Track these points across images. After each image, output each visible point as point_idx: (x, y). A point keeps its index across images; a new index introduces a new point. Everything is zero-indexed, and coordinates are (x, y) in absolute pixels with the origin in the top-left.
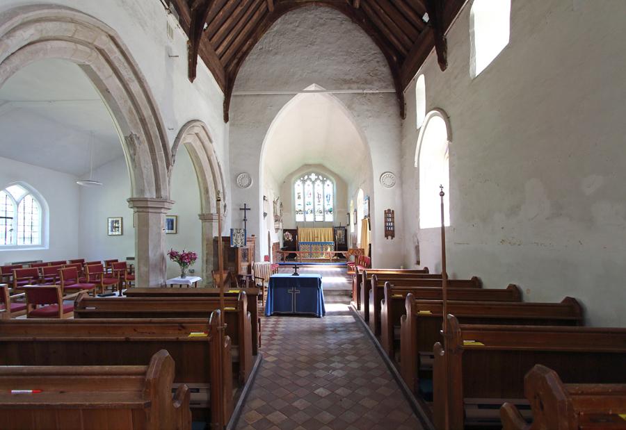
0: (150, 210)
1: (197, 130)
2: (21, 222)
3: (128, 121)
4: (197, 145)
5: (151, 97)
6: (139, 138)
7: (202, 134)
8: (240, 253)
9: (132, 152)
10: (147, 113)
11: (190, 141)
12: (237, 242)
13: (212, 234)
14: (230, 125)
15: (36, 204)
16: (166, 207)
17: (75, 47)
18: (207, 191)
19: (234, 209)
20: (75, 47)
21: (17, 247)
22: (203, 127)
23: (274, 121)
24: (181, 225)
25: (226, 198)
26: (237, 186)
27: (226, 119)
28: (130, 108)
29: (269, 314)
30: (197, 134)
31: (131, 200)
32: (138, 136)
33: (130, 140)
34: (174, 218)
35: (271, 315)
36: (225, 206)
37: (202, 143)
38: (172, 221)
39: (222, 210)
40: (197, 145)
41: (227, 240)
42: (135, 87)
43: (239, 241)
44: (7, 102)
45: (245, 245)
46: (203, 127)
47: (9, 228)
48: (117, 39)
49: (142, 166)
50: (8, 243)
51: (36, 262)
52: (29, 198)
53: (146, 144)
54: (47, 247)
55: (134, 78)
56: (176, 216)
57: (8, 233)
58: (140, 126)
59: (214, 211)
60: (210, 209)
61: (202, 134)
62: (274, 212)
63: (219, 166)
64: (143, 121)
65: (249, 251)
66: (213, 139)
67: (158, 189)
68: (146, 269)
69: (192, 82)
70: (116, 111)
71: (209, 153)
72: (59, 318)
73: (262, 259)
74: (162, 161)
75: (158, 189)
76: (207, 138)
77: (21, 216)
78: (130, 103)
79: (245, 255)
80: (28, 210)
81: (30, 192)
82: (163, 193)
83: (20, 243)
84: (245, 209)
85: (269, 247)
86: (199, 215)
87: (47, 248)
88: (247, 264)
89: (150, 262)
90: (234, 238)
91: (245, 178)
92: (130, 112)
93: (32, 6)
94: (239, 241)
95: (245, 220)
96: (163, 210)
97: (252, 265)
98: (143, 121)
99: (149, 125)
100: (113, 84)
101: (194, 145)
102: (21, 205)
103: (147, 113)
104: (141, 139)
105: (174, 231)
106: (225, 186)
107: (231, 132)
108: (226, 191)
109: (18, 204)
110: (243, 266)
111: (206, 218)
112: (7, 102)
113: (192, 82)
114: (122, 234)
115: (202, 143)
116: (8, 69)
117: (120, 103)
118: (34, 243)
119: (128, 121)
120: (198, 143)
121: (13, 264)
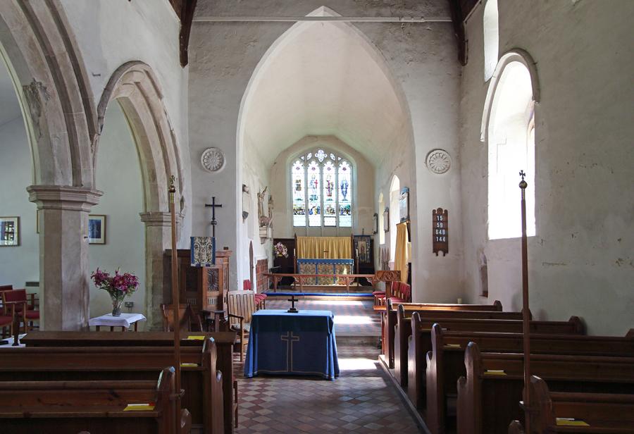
0: (64, 206)
1: (137, 77)
3: (28, 60)
4: (138, 102)
6: (45, 88)
7: (147, 85)
12: (201, 258)
13: (161, 245)
14: (192, 70)
16: (88, 200)
19: (195, 206)
22: (147, 72)
24: (113, 230)
25: (184, 188)
26: (201, 168)
27: (184, 61)
28: (32, 39)
29: (250, 374)
30: (137, 84)
31: (33, 190)
33: (32, 92)
35: (254, 376)
36: (182, 201)
37: (146, 98)
38: (98, 223)
39: (177, 208)
41: (186, 255)
43: (204, 257)
45: (214, 262)
46: (147, 72)
48: (151, 74)
56: (105, 216)
59: (164, 208)
61: (147, 85)
62: (259, 212)
64: (52, 60)
65: (220, 273)
66: (163, 92)
67: (76, 173)
71: (157, 115)
73: (241, 286)
74: (83, 128)
75: (76, 173)
79: (213, 280)
82: (84, 179)
85: (252, 267)
86: (142, 215)
88: (216, 293)
89: (64, 288)
90: (197, 251)
92: (32, 45)
93: (117, 70)
94: (204, 257)
95: (213, 223)
96: (83, 207)
97: (225, 295)
98: (52, 60)
99: (61, 68)
103: (58, 47)
105: (101, 240)
106: (182, 168)
107: (191, 81)
111: (152, 219)
114: (19, 244)
115: (146, 98)
120: (141, 99)
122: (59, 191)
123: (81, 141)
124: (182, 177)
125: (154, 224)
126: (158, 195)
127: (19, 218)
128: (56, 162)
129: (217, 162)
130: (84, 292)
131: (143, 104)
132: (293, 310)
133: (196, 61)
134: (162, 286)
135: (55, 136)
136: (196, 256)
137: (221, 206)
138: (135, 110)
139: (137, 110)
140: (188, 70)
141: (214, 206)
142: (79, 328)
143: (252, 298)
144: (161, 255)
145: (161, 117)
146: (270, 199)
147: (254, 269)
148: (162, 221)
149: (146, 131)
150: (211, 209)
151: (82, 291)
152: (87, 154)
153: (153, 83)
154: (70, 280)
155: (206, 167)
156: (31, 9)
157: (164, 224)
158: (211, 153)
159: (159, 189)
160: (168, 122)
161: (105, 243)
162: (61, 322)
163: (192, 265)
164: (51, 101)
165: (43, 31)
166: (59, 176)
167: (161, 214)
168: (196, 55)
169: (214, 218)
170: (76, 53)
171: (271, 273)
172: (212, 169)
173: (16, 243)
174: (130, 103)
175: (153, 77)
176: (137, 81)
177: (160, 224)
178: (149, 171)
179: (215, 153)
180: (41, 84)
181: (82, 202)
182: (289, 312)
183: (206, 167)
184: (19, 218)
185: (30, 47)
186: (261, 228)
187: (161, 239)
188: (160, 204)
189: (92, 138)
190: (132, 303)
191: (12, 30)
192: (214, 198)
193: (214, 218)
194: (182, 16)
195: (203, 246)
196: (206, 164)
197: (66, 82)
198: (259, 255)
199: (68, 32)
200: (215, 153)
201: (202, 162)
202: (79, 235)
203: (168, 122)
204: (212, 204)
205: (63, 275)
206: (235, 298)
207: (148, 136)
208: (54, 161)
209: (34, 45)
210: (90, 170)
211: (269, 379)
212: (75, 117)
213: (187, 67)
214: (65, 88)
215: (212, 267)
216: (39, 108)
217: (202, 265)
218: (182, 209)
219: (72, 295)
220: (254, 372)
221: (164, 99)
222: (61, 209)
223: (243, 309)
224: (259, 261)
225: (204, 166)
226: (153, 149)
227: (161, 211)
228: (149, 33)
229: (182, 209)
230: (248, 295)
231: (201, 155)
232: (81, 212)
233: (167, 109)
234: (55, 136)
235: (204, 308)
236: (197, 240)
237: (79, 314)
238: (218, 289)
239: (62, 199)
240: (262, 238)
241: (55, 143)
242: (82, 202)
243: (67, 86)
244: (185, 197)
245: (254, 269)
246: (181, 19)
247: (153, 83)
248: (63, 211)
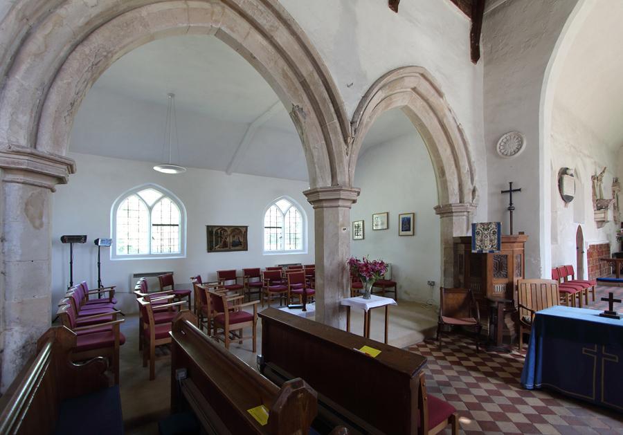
0: (325, 204)
1: (411, 82)
2: (287, 231)
3: (285, 90)
4: (418, 107)
5: (307, 45)
6: (302, 109)
7: (424, 87)
8: (490, 262)
9: (300, 132)
10: (306, 68)
11: (406, 104)
13: (452, 233)
14: (487, 64)
15: (298, 215)
16: (342, 197)
17: (185, 6)
18: (442, 173)
19: (491, 195)
20: (185, 6)
21: (284, 251)
22: (422, 75)
23: (571, 16)
24: (420, 224)
26: (497, 155)
27: (475, 56)
28: (283, 70)
30: (414, 89)
31: (307, 194)
32: (301, 107)
33: (295, 115)
34: (411, 216)
35: (535, 389)
37: (426, 101)
38: (409, 220)
40: (418, 107)
41: (467, 242)
42: (282, 37)
43: (487, 242)
44: (250, 124)
45: (499, 249)
46: (422, 75)
47: (279, 236)
48: (426, 75)
49: (311, 146)
50: (279, 248)
51: (296, 264)
52: (293, 209)
53: (313, 115)
54: (307, 252)
55: (277, 23)
56: (414, 214)
57: (279, 240)
58: (301, 91)
60: (448, 197)
61: (424, 87)
62: (594, 194)
63: (460, 131)
64: (304, 84)
66: (443, 90)
67: (334, 176)
68: (322, 282)
69: (396, 10)
70: (271, 81)
71: (440, 114)
72: (571, 267)
74: (336, 133)
75: (334, 176)
76: (433, 91)
77: (287, 225)
78: (282, 62)
79: (502, 266)
80: (293, 220)
81: (293, 204)
82: (340, 179)
83: (287, 248)
84: (511, 191)
87: (307, 252)
88: (506, 281)
89: (326, 272)
90: (478, 238)
91: (513, 138)
92: (285, 76)
93: (377, 81)
94: (487, 242)
95: (511, 209)
96: (340, 203)
98: (304, 84)
99: (312, 87)
100: (256, 42)
101: (412, 108)
102: (287, 215)
103: (306, 68)
104: (305, 110)
105: (411, 233)
106: (473, 159)
107: (486, 75)
108: (476, 167)
109: (284, 215)
110: (497, 287)
111: (444, 211)
112: (250, 124)
113: (396, 10)
114: (364, 238)
115: (426, 101)
116: (88, 52)
117: (270, 67)
118: (131, 253)
119: (285, 90)
120: (420, 102)
121: (269, 269)
122: (318, 192)
123: (336, 147)
124: (473, 168)
125: (445, 215)
126: (447, 189)
127: (363, 221)
128: (317, 169)
129: (514, 145)
130: (342, 276)
131: (424, 107)
132: (610, 314)
133: (491, 52)
134: (453, 270)
135: (315, 148)
136: (478, 243)
137: (519, 190)
138: (417, 116)
139: (420, 116)
140: (483, 65)
141: (511, 191)
142: (337, 305)
143: (554, 290)
144: (451, 242)
145: (445, 115)
146: (616, 182)
147: (585, 255)
148: (452, 212)
149: (431, 133)
150: (508, 195)
151: (341, 275)
152: (341, 156)
153: (432, 84)
154: (330, 265)
155: (503, 153)
156: (277, 43)
157: (454, 214)
158: (508, 138)
159: (449, 184)
160: (454, 118)
161: (413, 235)
162: (324, 299)
163: (473, 251)
164: (308, 119)
165: (291, 58)
166: (319, 180)
167: (450, 205)
168: (492, 47)
169: (511, 204)
170: (322, 67)
171: (615, 258)
172: (509, 154)
173: (361, 237)
174: (411, 110)
175: (430, 78)
176: (413, 87)
177: (450, 214)
178: (439, 169)
179: (512, 137)
180: (298, 106)
181: (338, 199)
182: (601, 315)
183: (503, 153)
184: (363, 221)
185: (284, 77)
186: (597, 212)
187: (452, 228)
188: (450, 197)
189: (346, 141)
190: (434, 282)
191: (268, 68)
192: (511, 183)
193: (511, 204)
194: (472, 14)
195: (486, 232)
196: (502, 151)
197: (317, 99)
198: (594, 237)
199: (312, 52)
200: (512, 137)
201: (498, 150)
202: (337, 227)
203: (454, 118)
204: (509, 189)
205: (325, 261)
206: (538, 288)
207: (434, 137)
208: (315, 168)
209: (286, 74)
210: (344, 171)
211: (559, 401)
212: (328, 127)
213: (481, 62)
214: (317, 103)
215: (497, 252)
216: (301, 128)
217: (484, 252)
218: (473, 198)
219: (332, 277)
220: (535, 382)
221: (447, 96)
222: (322, 207)
223: (534, 298)
224: (592, 247)
225: (500, 154)
226: (439, 148)
227: (450, 202)
228: (431, 37)
229: (473, 198)
230: (549, 286)
231: (498, 142)
232: (339, 208)
233: (452, 106)
234: (315, 148)
235: (489, 294)
236: (479, 227)
237: (337, 294)
238: (506, 276)
239: (321, 198)
240: (598, 222)
241: (316, 154)
242: (338, 199)
243: (319, 102)
244: (477, 187)
245: (585, 255)
246: (472, 18)
247: (432, 84)
248: (325, 209)
